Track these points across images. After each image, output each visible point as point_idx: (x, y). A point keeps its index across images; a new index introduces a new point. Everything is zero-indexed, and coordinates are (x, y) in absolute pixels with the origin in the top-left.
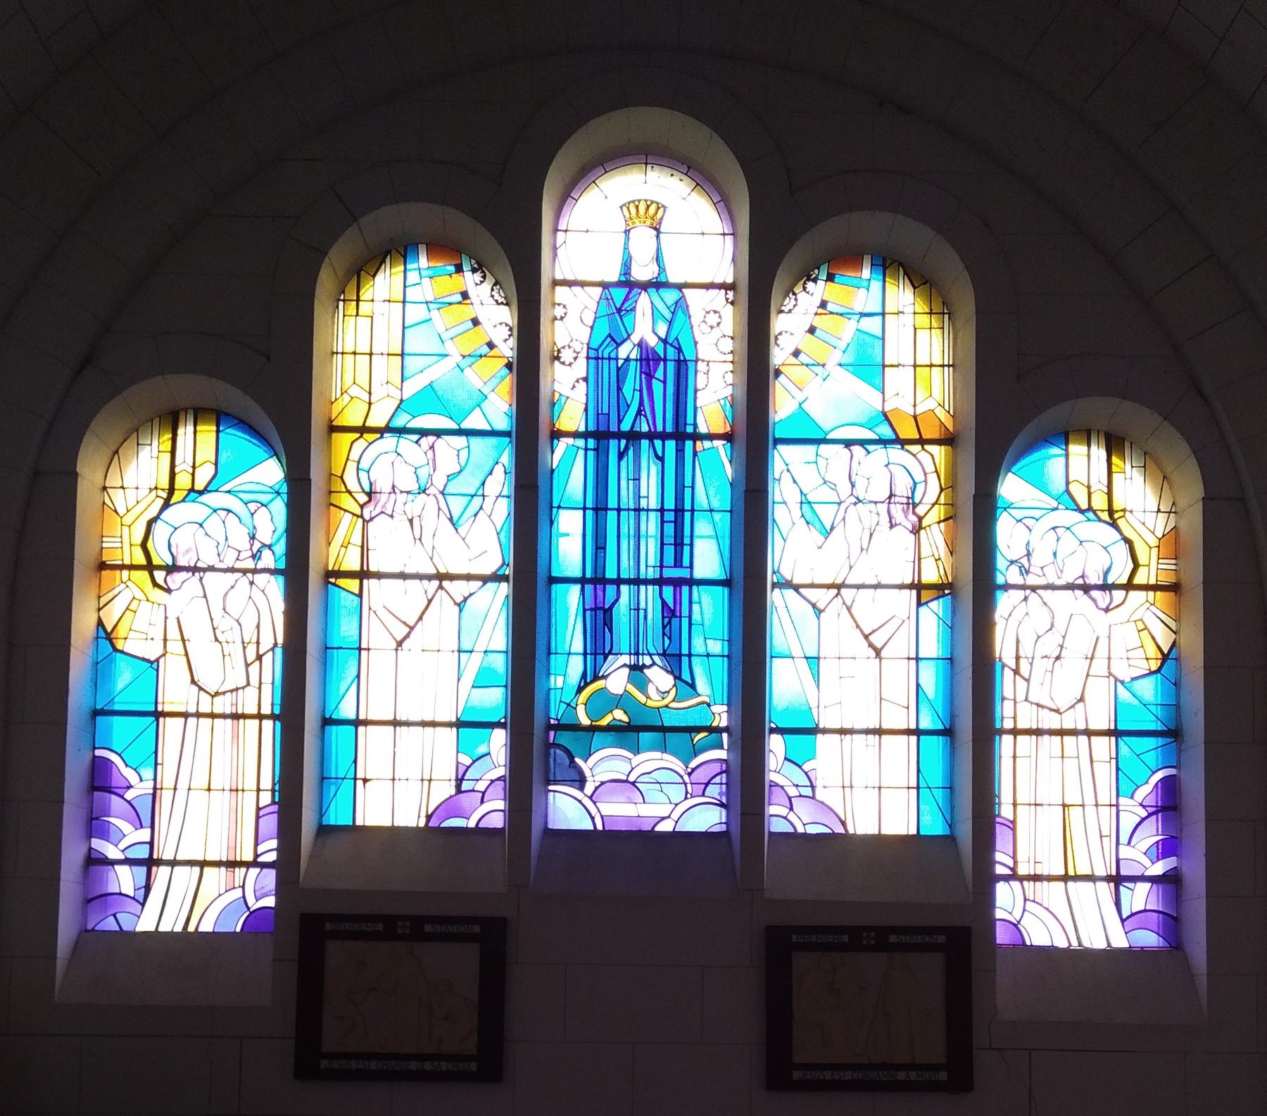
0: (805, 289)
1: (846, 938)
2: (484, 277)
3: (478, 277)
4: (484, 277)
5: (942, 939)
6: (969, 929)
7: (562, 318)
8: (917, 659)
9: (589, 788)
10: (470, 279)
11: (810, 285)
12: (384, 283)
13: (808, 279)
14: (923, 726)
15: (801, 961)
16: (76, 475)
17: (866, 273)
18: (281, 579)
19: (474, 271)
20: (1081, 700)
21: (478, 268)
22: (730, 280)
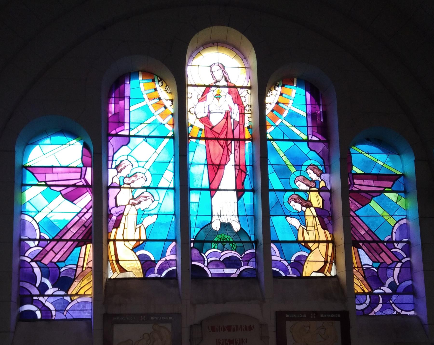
0: (275, 89)
1: (305, 316)
2: (163, 84)
3: (160, 83)
4: (163, 84)
5: (339, 316)
6: (276, 312)
7: (190, 98)
8: (197, 215)
9: (206, 263)
10: (157, 85)
11: (277, 88)
12: (302, 91)
13: (276, 85)
14: (321, 239)
15: (289, 324)
16: (15, 151)
17: (141, 78)
18: (235, 192)
19: (159, 81)
20: (145, 229)
21: (161, 80)
22: (249, 85)
